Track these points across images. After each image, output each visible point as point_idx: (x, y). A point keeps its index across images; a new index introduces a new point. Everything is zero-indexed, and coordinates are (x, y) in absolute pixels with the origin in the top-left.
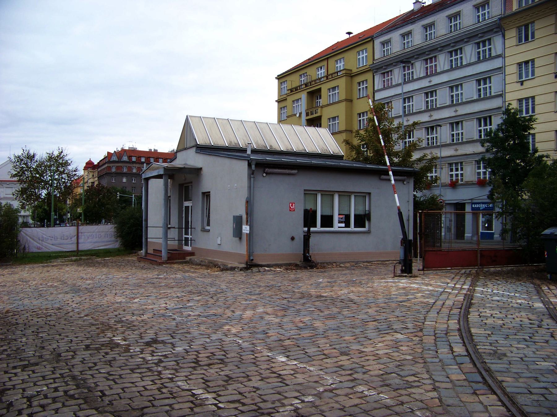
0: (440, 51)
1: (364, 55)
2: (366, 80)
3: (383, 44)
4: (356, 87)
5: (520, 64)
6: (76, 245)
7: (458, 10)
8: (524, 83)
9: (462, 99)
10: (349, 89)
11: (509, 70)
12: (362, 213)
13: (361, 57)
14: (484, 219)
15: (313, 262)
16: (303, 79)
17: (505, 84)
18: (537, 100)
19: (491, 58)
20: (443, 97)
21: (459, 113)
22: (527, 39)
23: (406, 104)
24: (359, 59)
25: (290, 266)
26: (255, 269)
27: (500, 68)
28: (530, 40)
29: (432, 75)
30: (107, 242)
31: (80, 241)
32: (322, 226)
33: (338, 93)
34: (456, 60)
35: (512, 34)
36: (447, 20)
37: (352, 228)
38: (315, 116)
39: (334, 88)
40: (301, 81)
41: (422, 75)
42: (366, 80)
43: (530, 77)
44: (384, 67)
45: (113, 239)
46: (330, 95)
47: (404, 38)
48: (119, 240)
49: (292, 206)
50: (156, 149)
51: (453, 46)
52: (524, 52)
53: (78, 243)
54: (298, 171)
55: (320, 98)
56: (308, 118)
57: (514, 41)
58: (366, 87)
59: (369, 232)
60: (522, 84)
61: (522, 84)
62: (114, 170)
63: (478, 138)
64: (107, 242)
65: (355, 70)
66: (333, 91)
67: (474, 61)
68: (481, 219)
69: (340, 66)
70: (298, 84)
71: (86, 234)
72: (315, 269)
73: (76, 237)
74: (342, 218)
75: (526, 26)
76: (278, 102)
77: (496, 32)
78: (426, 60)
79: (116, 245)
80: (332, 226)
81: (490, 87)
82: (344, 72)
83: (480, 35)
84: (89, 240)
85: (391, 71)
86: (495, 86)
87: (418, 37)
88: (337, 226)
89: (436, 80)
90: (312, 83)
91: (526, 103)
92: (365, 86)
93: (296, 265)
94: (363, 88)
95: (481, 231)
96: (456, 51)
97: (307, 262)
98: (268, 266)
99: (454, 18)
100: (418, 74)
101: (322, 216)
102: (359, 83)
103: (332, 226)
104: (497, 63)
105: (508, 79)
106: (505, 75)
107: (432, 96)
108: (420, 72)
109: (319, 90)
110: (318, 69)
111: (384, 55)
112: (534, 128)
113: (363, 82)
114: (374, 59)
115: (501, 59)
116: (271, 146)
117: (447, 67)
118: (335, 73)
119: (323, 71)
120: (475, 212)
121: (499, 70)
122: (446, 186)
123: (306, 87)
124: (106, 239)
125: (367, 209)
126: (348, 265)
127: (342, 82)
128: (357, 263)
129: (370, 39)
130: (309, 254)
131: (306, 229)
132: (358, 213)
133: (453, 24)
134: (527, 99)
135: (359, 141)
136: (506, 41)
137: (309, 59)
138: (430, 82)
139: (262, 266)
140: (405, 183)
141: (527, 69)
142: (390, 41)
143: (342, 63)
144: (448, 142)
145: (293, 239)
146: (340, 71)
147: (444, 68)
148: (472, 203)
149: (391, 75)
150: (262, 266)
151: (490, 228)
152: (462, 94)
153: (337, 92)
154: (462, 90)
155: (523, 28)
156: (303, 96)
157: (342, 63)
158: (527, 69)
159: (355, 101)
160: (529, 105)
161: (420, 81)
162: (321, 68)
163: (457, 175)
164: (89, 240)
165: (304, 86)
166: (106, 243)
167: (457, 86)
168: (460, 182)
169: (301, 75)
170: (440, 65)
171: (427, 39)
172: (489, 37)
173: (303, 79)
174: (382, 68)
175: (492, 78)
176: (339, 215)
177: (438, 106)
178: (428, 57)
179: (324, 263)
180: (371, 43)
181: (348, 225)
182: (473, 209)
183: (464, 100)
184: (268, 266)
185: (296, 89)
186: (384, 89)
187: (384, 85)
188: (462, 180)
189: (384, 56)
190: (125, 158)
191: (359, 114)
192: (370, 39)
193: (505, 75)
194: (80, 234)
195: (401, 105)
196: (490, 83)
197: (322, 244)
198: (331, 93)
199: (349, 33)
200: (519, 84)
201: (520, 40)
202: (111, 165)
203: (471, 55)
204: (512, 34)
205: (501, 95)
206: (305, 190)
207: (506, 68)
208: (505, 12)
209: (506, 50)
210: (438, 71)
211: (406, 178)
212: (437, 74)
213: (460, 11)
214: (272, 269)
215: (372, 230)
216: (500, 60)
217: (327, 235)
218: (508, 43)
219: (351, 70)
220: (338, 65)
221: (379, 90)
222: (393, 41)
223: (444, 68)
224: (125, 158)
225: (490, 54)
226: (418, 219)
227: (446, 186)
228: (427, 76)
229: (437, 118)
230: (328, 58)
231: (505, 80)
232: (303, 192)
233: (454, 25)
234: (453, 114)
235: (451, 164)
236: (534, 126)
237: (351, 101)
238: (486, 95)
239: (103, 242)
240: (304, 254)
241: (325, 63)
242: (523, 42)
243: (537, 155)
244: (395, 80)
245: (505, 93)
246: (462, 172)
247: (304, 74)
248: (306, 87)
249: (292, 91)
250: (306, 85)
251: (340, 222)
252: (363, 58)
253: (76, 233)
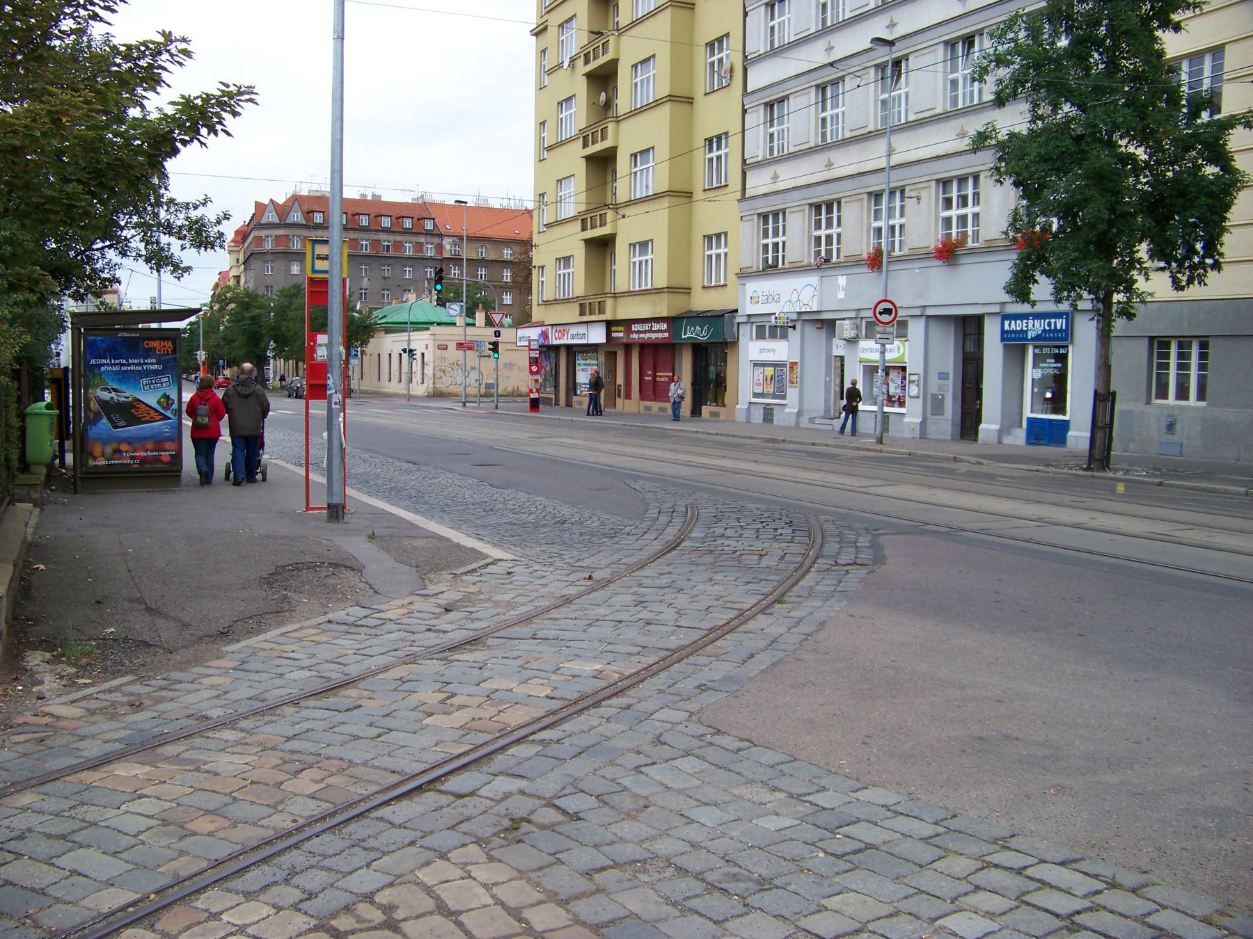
14: (1038, 374)
38: (602, 60)
50: (378, 192)
62: (268, 246)
68: (1031, 373)
76: (536, 35)
80: (1064, 414)
95: (1027, 413)
120: (1015, 345)
122: (926, 256)
144: (939, 110)
148: (1005, 317)
151: (1058, 402)
163: (963, 219)
168: (970, 244)
182: (1005, 336)
188: (976, 234)
190: (296, 217)
191: (710, 45)
202: (263, 233)
224: (296, 217)
226: (165, 325)
227: (926, 256)
235: (945, 183)
246: (976, 209)
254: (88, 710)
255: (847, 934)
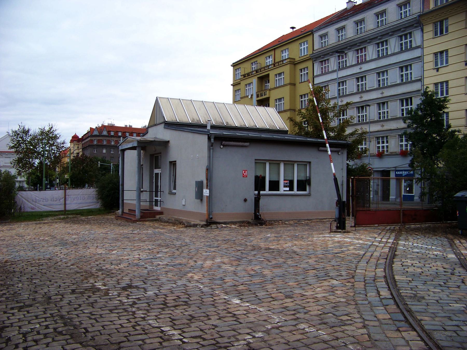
0: (369, 43)
1: (306, 46)
2: (307, 68)
3: (321, 37)
4: (298, 73)
5: (436, 54)
6: (64, 205)
7: (384, 9)
8: (440, 70)
9: (387, 83)
10: (293, 75)
11: (426, 59)
12: (303, 179)
13: (302, 47)
14: (406, 184)
15: (263, 220)
16: (254, 66)
17: (423, 71)
18: (451, 84)
19: (412, 49)
20: (371, 81)
21: (385, 95)
22: (441, 32)
23: (341, 88)
24: (301, 49)
25: (243, 224)
26: (214, 226)
27: (419, 57)
28: (444, 33)
29: (362, 63)
30: (90, 203)
31: (67, 202)
32: (270, 190)
33: (283, 78)
34: (383, 50)
35: (429, 28)
36: (374, 17)
37: (295, 191)
38: (264, 97)
39: (280, 74)
40: (253, 68)
41: (354, 63)
42: (307, 68)
43: (444, 65)
44: (322, 57)
45: (95, 200)
46: (276, 80)
47: (339, 32)
48: (100, 201)
49: (245, 173)
50: (131, 125)
51: (380, 38)
52: (440, 44)
53: (65, 204)
54: (250, 143)
55: (269, 82)
56: (258, 99)
57: (431, 35)
58: (307, 73)
59: (309, 195)
60: (438, 71)
61: (438, 71)
62: (95, 143)
63: (401, 116)
64: (90, 203)
65: (297, 59)
66: (279, 76)
67: (397, 51)
68: (403, 184)
69: (285, 56)
70: (250, 71)
71: (72, 196)
72: (264, 226)
73: (63, 199)
74: (286, 183)
75: (441, 22)
76: (233, 86)
77: (416, 27)
78: (357, 50)
79: (98, 206)
80: (278, 190)
81: (411, 73)
82: (288, 60)
83: (402, 30)
84: (75, 202)
85: (328, 60)
86: (415, 72)
87: (350, 31)
88: (283, 189)
89: (366, 67)
90: (262, 70)
91: (441, 86)
92: (306, 72)
93: (249, 223)
94: (304, 74)
95: (403, 194)
96: (382, 43)
97: (258, 220)
98: (225, 223)
99: (381, 15)
100: (351, 62)
101: (270, 182)
102: (301, 70)
103: (278, 190)
104: (417, 53)
105: (426, 67)
106: (423, 63)
107: (362, 81)
108: (352, 60)
109: (268, 76)
110: (266, 58)
111: (322, 46)
112: (447, 108)
113: (304, 69)
114: (313, 50)
115: (420, 49)
116: (227, 123)
117: (375, 56)
118: (281, 61)
119: (271, 60)
120: (399, 178)
121: (418, 59)
122: (374, 156)
123: (256, 73)
124: (89, 201)
125: (308, 175)
126: (292, 222)
127: (286, 69)
128: (299, 220)
129: (310, 33)
130: (259, 213)
131: (256, 192)
132: (300, 179)
133: (379, 20)
134: (442, 83)
135: (301, 118)
136: (424, 34)
137: (259, 50)
138: (361, 68)
139: (219, 223)
140: (340, 153)
141: (442, 58)
142: (327, 35)
143: (287, 53)
144: (376, 120)
145: (245, 200)
146: (285, 60)
147: (372, 57)
148: (396, 171)
149: (328, 63)
150: (219, 223)
151: (411, 191)
152: (387, 79)
153: (282, 77)
154: (387, 75)
155: (439, 23)
156: (254, 80)
157: (287, 53)
158: (442, 58)
159: (298, 85)
160: (443, 88)
161: (352, 68)
162: (269, 57)
163: (383, 147)
164: (75, 202)
165: (255, 72)
166: (89, 204)
167: (383, 72)
168: (385, 153)
169: (252, 63)
170: (369, 54)
171: (358, 33)
172: (410, 31)
173: (254, 66)
174: (320, 57)
175: (412, 65)
176: (284, 180)
177: (367, 89)
178: (359, 48)
179: (271, 221)
180: (311, 36)
181: (291, 189)
182: (396, 175)
183: (389, 84)
184: (225, 223)
185: (248, 74)
186: (322, 74)
187: (322, 72)
188: (387, 151)
189: (322, 47)
190: (105, 133)
191: (301, 96)
192: (310, 33)
193: (423, 63)
194: (67, 197)
195: (336, 88)
196: (411, 69)
197: (270, 205)
198: (277, 78)
199: (293, 28)
200: (435, 70)
201: (436, 34)
202: (93, 138)
203: (395, 46)
204: (429, 28)
205: (420, 80)
206: (255, 159)
207: (424, 57)
208: (423, 10)
209: (424, 42)
210: (367, 59)
211: (340, 149)
212: (367, 62)
213: (386, 9)
214: (228, 225)
215: (312, 193)
216: (419, 50)
217: (274, 197)
218: (426, 36)
219: (294, 59)
220: (284, 55)
221: (318, 76)
222: (329, 34)
223: (372, 57)
224: (105, 133)
225: (411, 46)
227: (374, 156)
228: (358, 64)
229: (367, 99)
230: (275, 49)
231: (423, 67)
232: (254, 161)
233: (381, 21)
234: (380, 96)
235: (378, 138)
236: (448, 106)
237: (294, 85)
238: (408, 80)
239: (86, 203)
240: (255, 214)
241: (272, 53)
242: (439, 35)
243: (450, 130)
244: (331, 67)
245: (423, 78)
246: (387, 144)
247: (255, 62)
248: (256, 73)
249: (244, 77)
250: (257, 71)
251: (285, 186)
252: (304, 48)
253: (64, 196)
254: (76, 297)
255: (325, 349)
